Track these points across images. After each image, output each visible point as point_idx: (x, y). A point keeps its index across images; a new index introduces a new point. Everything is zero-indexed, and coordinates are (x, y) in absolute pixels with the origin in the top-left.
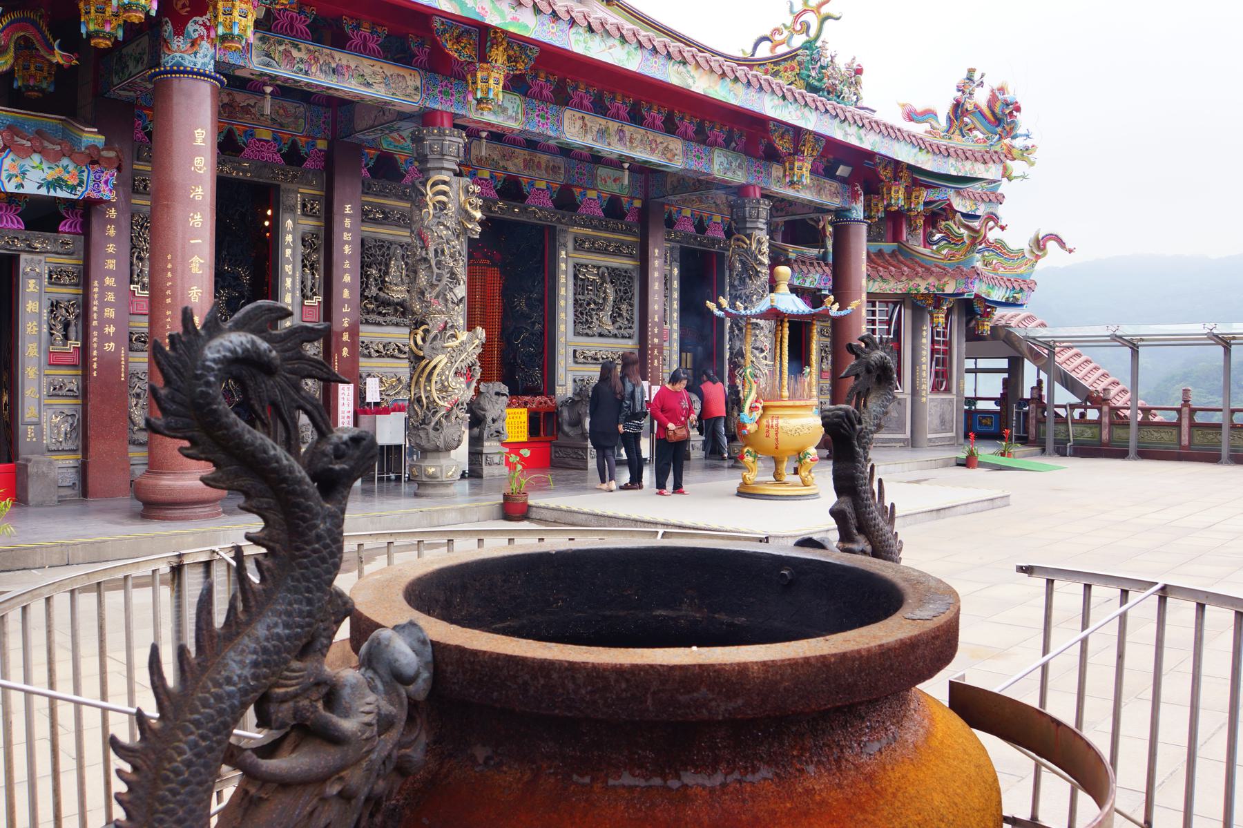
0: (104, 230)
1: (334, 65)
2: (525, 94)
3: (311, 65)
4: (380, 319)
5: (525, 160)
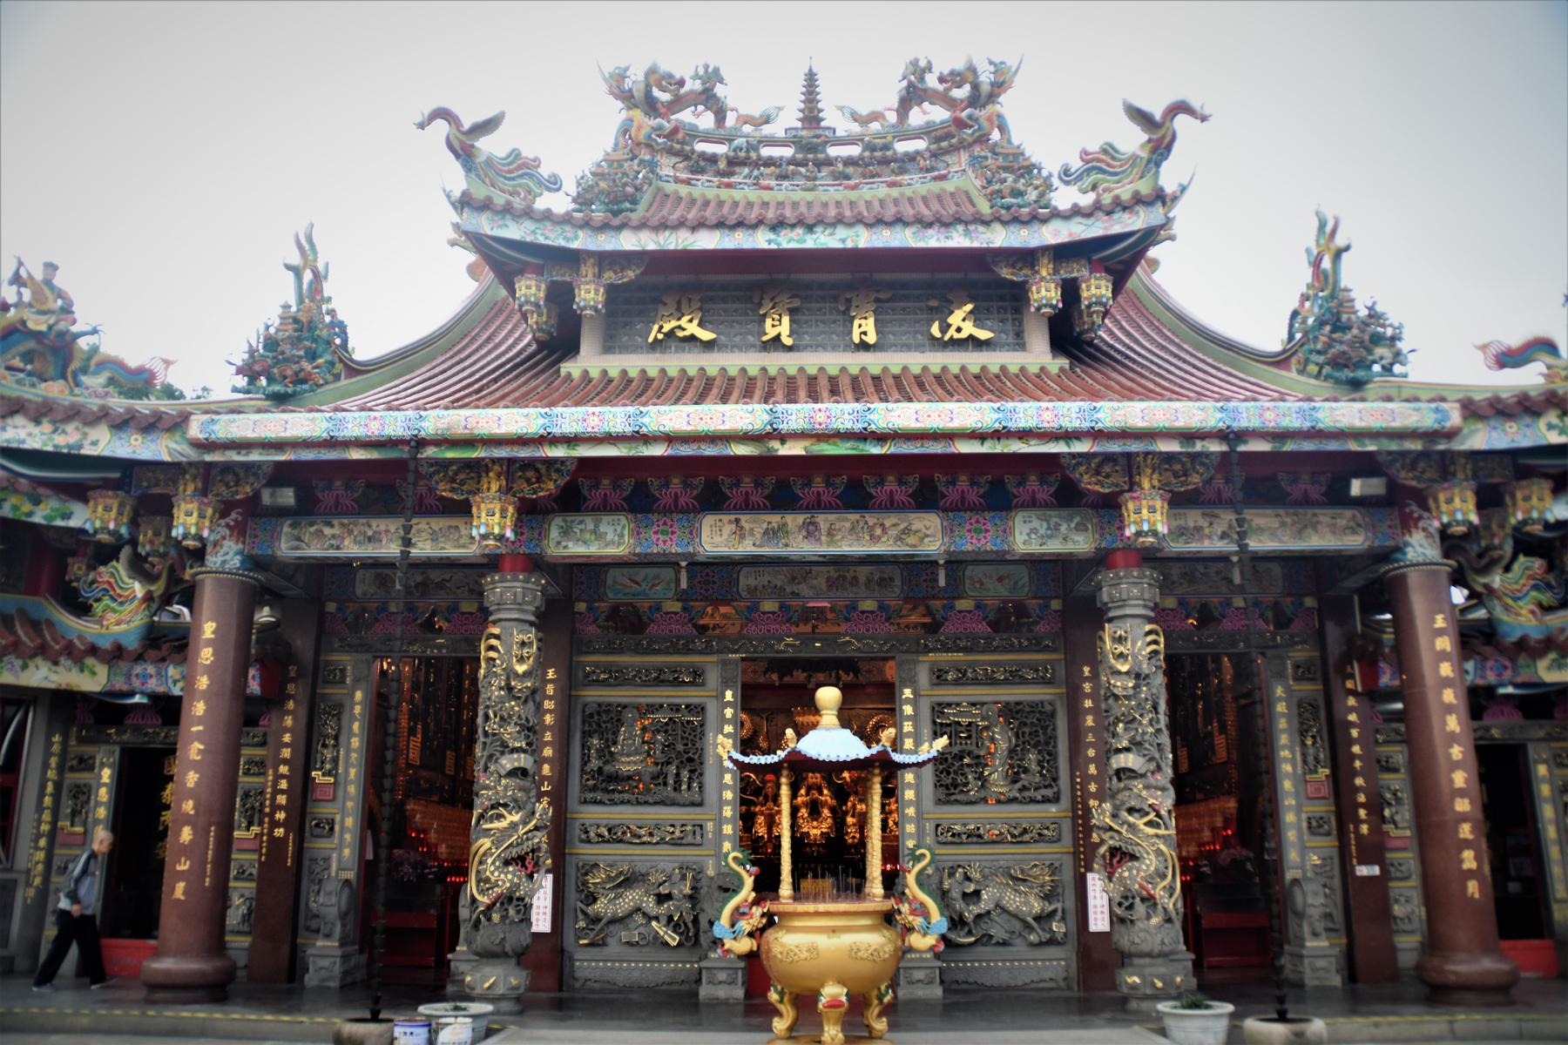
0: (282, 720)
1: (370, 533)
2: (945, 510)
3: (343, 539)
4: (605, 797)
5: (828, 579)
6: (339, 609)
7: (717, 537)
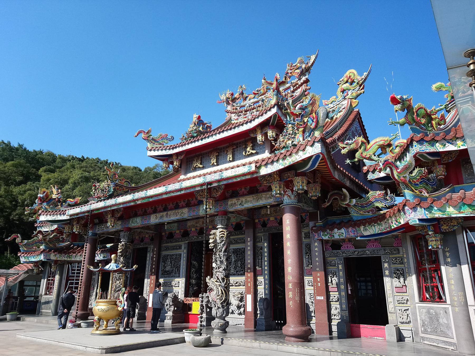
6: (259, 221)
7: (154, 220)
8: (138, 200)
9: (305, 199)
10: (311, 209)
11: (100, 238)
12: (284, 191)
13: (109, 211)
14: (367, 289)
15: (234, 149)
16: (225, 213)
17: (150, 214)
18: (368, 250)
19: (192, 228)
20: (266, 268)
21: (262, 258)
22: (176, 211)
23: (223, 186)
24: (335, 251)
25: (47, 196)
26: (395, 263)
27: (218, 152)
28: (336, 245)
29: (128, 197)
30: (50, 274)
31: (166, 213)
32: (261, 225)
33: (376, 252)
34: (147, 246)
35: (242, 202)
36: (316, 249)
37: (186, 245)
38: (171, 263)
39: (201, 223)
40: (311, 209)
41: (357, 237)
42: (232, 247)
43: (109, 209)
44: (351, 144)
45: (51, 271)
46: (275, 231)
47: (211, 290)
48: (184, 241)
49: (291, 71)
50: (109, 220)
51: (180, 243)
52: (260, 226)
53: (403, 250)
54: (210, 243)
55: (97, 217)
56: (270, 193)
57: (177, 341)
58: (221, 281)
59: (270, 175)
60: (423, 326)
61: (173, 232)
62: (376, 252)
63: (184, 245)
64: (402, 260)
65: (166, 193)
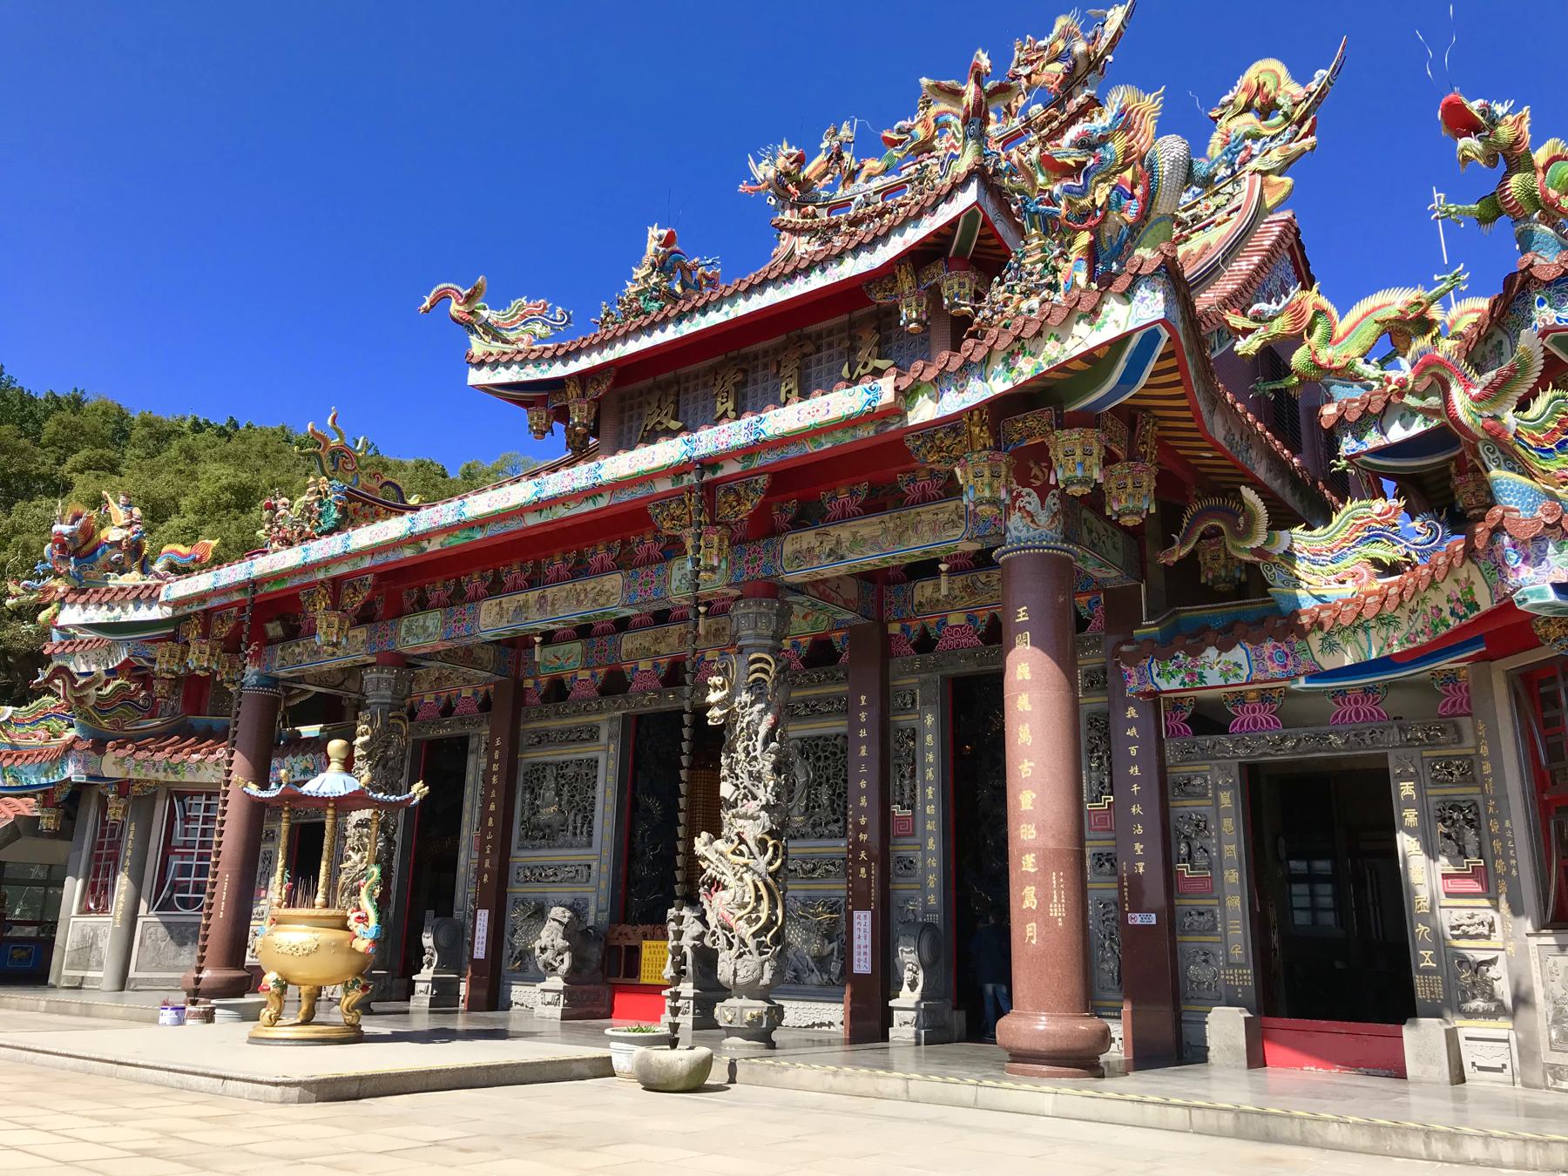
6: (903, 630)
7: (492, 619)
8: (427, 535)
9: (1090, 531)
10: (1114, 573)
11: (289, 698)
12: (1010, 492)
13: (322, 582)
14: (1314, 909)
15: (805, 355)
16: (772, 590)
17: (478, 598)
18: (1338, 733)
19: (641, 653)
20: (931, 810)
21: (914, 771)
22: (579, 586)
23: (763, 480)
24: (1207, 741)
25: (88, 533)
26: (1442, 781)
27: (745, 371)
28: (1208, 719)
29: (394, 528)
30: (103, 835)
31: (537, 593)
32: (914, 646)
33: (1367, 737)
34: (468, 729)
35: (838, 542)
36: (1132, 732)
37: (617, 727)
38: (558, 794)
39: (674, 640)
40: (1111, 575)
41: (1293, 678)
42: (798, 730)
43: (321, 576)
44: (1272, 319)
45: (104, 823)
46: (967, 667)
47: (716, 885)
48: (608, 710)
49: (1028, 70)
50: (321, 623)
51: (593, 718)
52: (908, 648)
53: (1475, 729)
54: (709, 707)
55: (274, 611)
56: (952, 505)
57: (577, 1068)
58: (755, 850)
59: (952, 424)
60: (1555, 1021)
61: (567, 677)
62: (1367, 737)
63: (607, 722)
64: (1471, 766)
65: (538, 506)
